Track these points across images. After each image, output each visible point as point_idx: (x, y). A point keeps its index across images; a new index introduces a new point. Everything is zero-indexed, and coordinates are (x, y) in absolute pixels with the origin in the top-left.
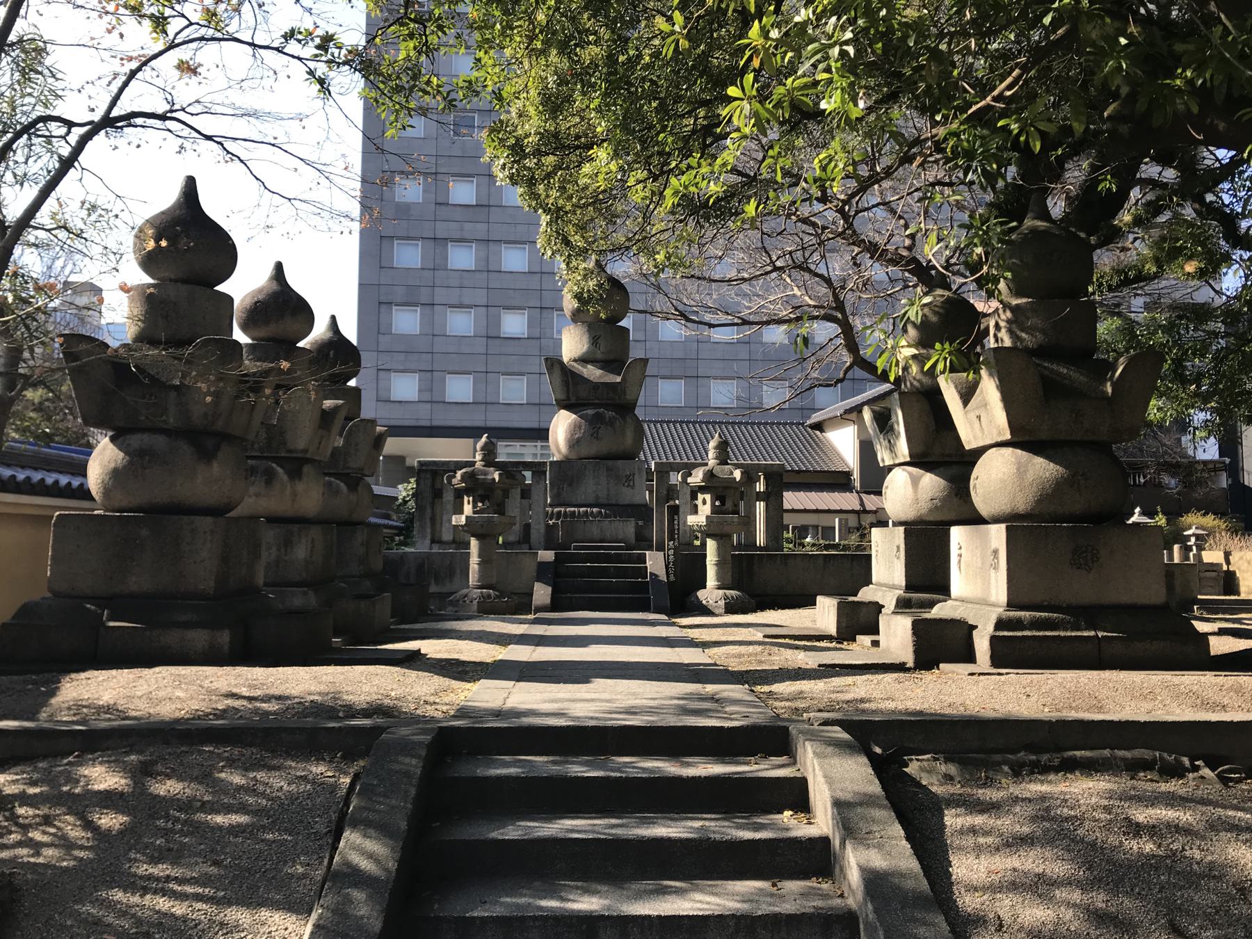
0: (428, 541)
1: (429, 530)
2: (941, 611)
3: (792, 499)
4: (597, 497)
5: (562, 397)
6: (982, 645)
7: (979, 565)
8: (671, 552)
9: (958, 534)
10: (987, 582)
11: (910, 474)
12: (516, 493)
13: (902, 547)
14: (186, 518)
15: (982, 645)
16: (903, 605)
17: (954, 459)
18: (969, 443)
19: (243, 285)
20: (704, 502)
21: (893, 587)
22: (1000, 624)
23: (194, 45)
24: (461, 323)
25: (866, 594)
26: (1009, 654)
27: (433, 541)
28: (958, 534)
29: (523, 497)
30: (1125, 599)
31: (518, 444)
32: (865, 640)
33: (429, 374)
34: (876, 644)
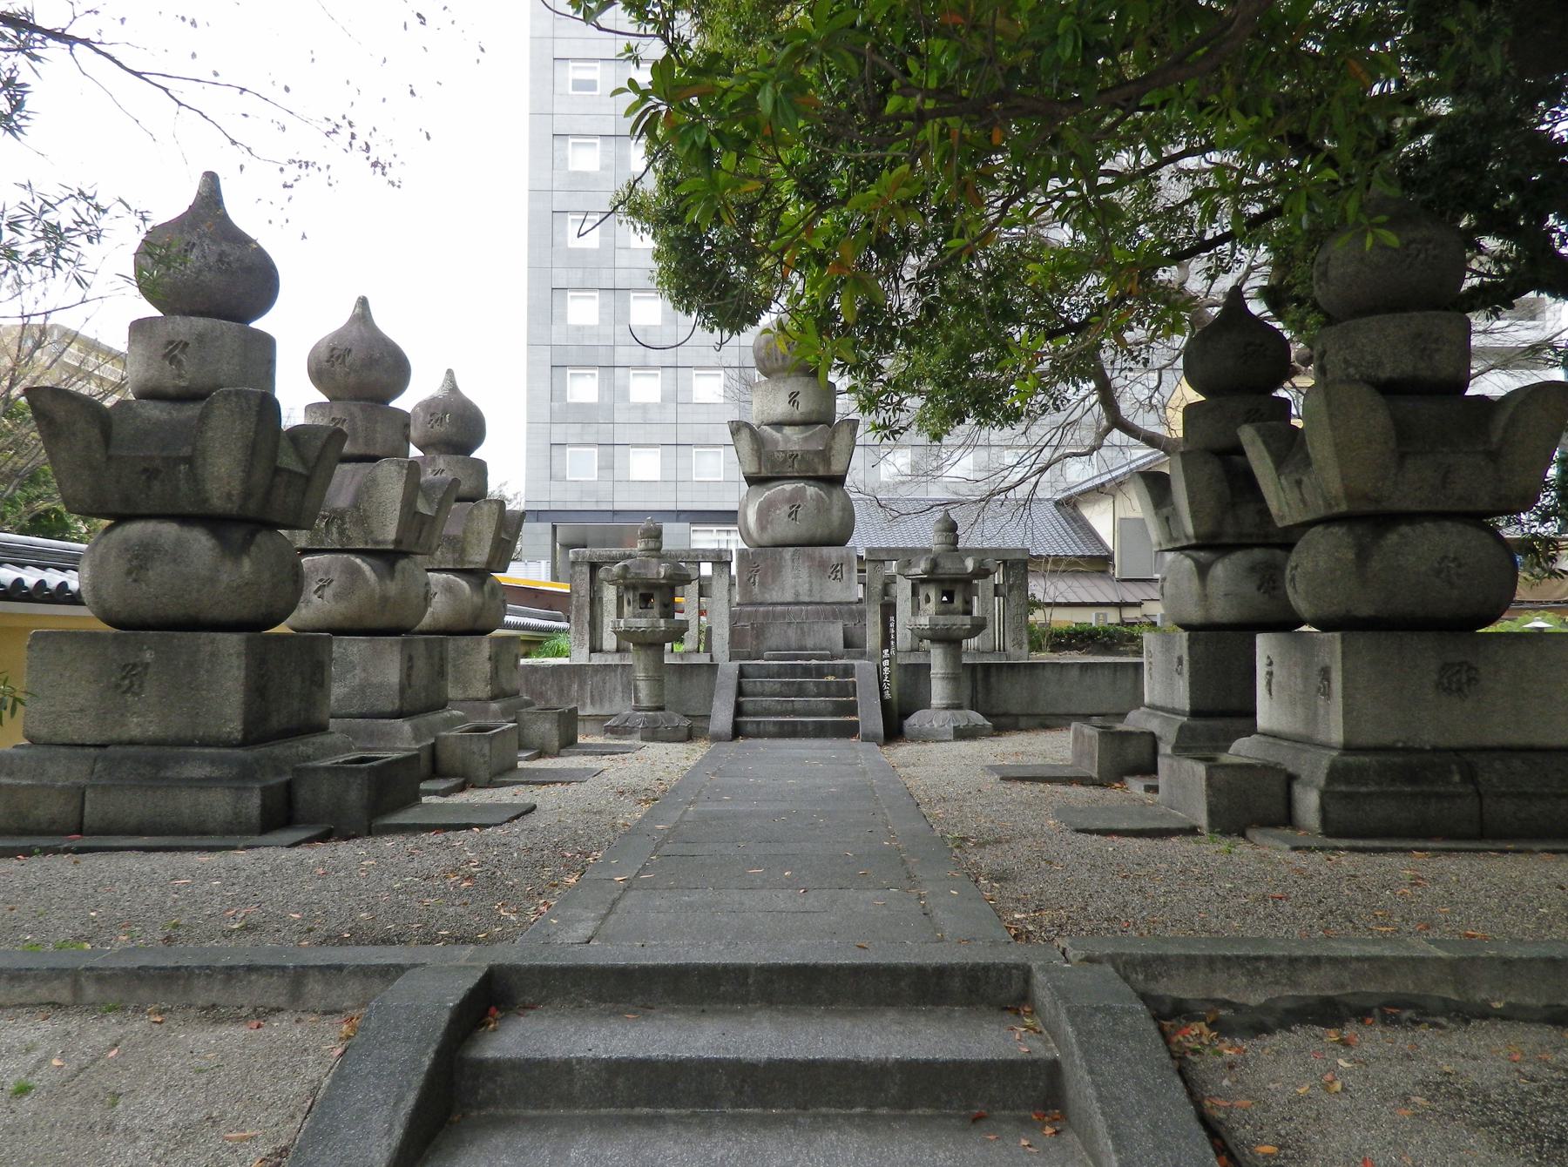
0: (586, 650)
1: (587, 637)
2: (1242, 750)
3: (1038, 588)
4: (797, 594)
5: (752, 469)
6: (1308, 802)
7: (1300, 687)
8: (886, 663)
9: (1264, 645)
10: (1312, 718)
11: (1196, 561)
12: (693, 588)
13: (1186, 658)
14: (204, 636)
15: (1308, 802)
16: (1186, 745)
17: (1255, 540)
18: (1282, 518)
19: (296, 328)
20: (928, 600)
21: (1174, 711)
22: (1334, 774)
23: (1058, 466)
24: (645, 389)
25: (1136, 721)
26: (1349, 823)
27: (593, 650)
28: (1264, 645)
29: (701, 595)
30: (1517, 738)
31: (715, 529)
32: (1136, 786)
33: (610, 449)
34: (1153, 789)
